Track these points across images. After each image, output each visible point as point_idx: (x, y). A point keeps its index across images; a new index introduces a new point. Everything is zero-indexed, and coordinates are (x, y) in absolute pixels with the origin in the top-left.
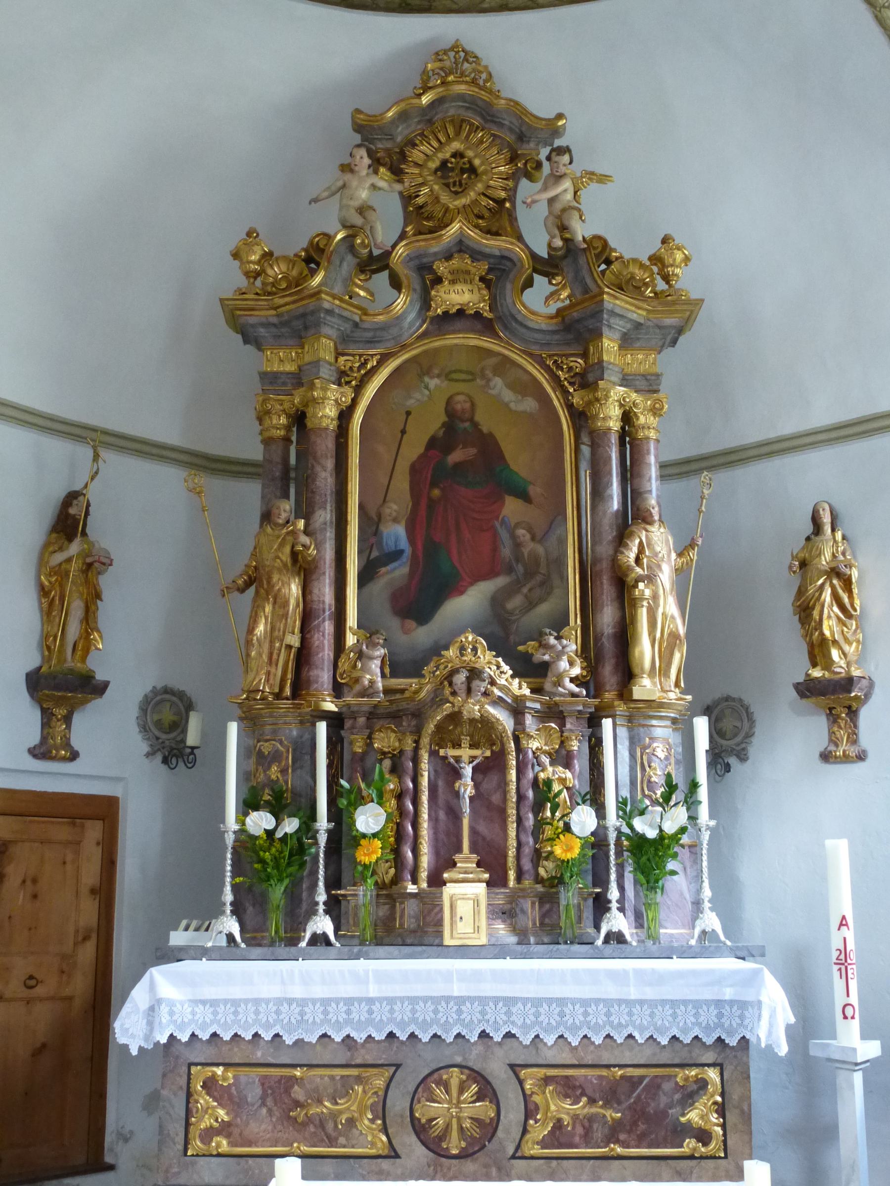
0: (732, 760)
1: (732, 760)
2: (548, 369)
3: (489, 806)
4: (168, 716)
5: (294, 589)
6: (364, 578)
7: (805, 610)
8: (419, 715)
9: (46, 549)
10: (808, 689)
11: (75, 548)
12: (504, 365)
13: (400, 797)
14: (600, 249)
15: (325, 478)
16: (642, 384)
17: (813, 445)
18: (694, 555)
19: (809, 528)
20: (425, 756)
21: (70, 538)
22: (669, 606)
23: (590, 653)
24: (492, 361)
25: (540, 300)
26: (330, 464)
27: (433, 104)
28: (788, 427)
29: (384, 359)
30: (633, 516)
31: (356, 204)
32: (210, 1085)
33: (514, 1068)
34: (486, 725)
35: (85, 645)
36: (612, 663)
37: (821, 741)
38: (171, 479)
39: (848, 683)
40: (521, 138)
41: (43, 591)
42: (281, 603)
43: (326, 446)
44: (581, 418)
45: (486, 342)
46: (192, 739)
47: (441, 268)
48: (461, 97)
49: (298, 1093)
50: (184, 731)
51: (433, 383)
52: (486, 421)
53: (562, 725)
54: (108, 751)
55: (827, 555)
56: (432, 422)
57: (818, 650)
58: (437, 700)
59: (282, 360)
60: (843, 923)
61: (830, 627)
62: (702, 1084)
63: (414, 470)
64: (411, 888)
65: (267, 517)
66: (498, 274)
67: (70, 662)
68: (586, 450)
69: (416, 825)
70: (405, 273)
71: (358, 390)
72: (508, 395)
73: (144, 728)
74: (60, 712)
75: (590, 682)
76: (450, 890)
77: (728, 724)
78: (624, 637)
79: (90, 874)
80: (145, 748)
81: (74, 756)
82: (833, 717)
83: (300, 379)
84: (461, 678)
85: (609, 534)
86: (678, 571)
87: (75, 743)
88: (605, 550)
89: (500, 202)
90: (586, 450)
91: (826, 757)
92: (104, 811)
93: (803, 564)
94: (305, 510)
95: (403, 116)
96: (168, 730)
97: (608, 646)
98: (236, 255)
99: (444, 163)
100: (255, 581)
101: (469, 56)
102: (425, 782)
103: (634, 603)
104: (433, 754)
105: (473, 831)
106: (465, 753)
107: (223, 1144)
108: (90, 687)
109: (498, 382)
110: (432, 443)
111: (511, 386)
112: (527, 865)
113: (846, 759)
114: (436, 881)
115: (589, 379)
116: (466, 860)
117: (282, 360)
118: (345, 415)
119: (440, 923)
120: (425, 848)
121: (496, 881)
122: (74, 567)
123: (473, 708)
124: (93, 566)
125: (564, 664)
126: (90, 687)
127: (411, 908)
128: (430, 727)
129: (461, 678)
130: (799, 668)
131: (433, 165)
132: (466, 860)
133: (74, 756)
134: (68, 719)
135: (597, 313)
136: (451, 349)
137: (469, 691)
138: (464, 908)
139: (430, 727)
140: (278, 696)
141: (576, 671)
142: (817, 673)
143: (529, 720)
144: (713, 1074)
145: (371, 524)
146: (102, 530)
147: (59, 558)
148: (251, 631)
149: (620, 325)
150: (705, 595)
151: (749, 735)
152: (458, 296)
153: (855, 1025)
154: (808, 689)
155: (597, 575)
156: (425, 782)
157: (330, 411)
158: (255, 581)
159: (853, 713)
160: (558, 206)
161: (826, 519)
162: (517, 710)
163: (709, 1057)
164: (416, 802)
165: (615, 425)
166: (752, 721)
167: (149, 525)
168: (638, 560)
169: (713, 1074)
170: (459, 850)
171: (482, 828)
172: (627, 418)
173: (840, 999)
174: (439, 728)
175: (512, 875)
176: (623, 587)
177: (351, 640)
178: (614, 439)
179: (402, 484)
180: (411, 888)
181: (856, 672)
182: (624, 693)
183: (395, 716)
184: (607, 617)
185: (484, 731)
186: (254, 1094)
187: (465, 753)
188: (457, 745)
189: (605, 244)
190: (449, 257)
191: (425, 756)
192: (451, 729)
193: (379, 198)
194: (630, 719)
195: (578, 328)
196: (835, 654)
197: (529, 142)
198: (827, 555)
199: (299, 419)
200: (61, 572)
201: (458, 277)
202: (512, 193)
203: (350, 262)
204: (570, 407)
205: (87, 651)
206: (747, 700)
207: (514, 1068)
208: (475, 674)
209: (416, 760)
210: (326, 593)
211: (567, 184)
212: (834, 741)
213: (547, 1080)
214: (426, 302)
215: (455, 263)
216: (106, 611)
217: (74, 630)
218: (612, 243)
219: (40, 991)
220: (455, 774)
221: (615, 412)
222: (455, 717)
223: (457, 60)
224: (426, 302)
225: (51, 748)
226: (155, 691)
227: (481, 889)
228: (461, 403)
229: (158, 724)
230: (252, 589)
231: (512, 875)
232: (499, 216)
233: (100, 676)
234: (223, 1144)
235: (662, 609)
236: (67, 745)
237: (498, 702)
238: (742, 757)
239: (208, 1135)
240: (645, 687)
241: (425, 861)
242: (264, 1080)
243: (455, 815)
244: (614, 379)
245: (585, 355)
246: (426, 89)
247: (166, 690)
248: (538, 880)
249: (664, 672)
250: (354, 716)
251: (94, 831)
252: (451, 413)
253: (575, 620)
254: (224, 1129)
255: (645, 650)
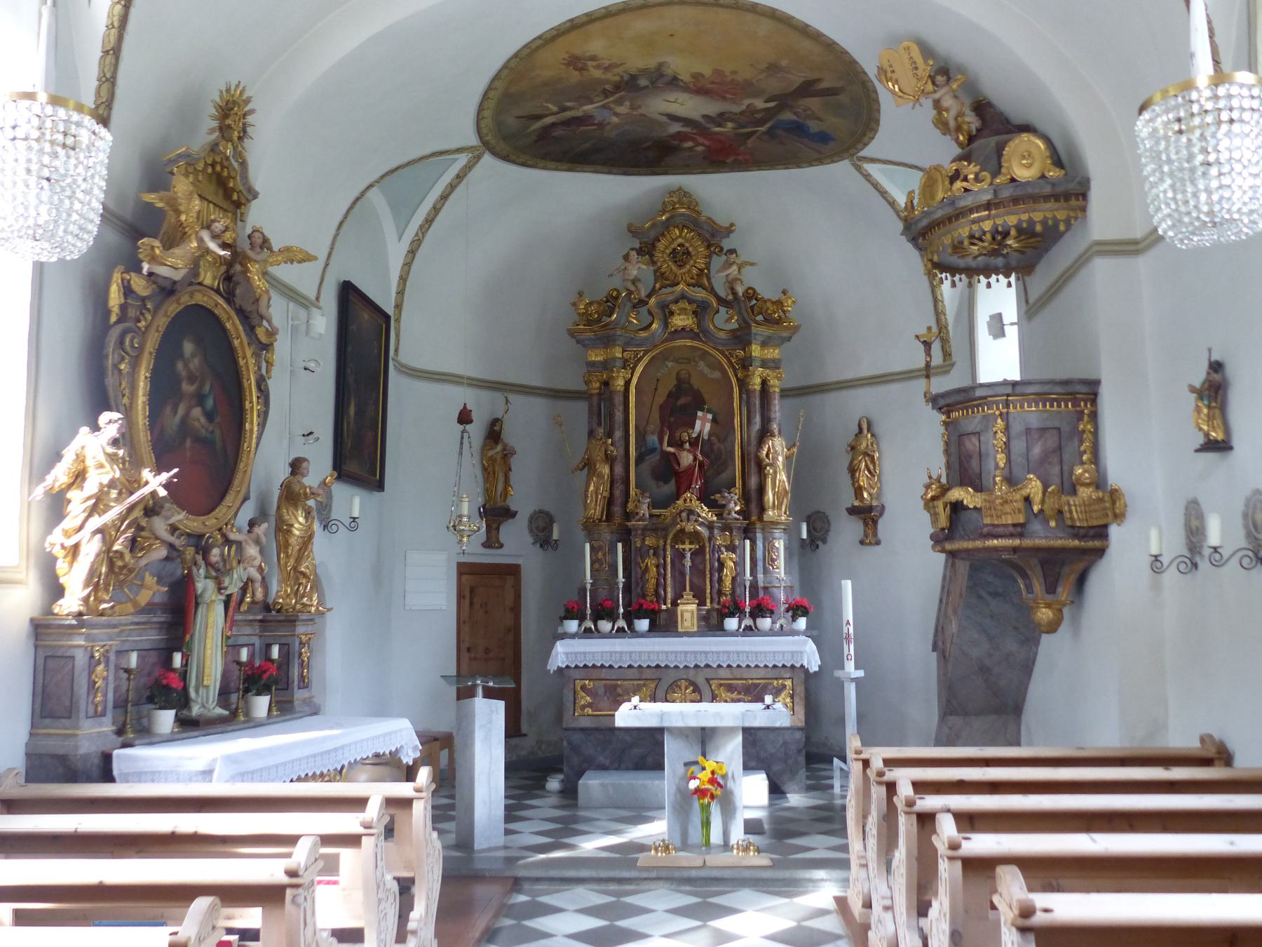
0: (820, 543)
1: (820, 543)
2: (725, 356)
3: (698, 571)
4: (541, 524)
5: (606, 470)
6: (639, 461)
7: (853, 471)
8: (666, 530)
9: (484, 448)
10: (853, 511)
11: (499, 448)
12: (705, 354)
13: (657, 567)
14: (751, 294)
15: (619, 415)
16: (772, 365)
17: (862, 385)
18: (795, 450)
19: (857, 430)
20: (668, 547)
21: (497, 443)
22: (782, 476)
23: (745, 497)
24: (699, 353)
25: (724, 322)
26: (621, 408)
27: (667, 219)
28: (850, 375)
29: (646, 353)
30: (765, 433)
31: (632, 277)
32: (583, 688)
33: (708, 680)
34: (697, 533)
35: (505, 494)
36: (754, 501)
37: (861, 535)
38: (538, 405)
39: (871, 508)
40: (713, 235)
41: (484, 469)
42: (600, 476)
43: (618, 399)
44: (743, 384)
45: (696, 344)
46: (555, 536)
47: (674, 307)
48: (682, 215)
49: (619, 691)
50: (551, 531)
51: (670, 364)
52: (696, 383)
53: (731, 533)
54: (516, 543)
55: (864, 445)
56: (669, 385)
57: (858, 491)
58: (674, 523)
59: (596, 356)
60: (848, 623)
61: (863, 482)
62: (784, 687)
63: (661, 408)
64: (664, 607)
65: (591, 434)
66: (701, 311)
67: (500, 503)
68: (744, 396)
69: (665, 579)
70: (655, 311)
71: (633, 370)
72: (706, 370)
73: (531, 531)
74: (495, 526)
75: (744, 513)
76: (680, 608)
77: (818, 525)
78: (761, 490)
79: (509, 602)
80: (531, 540)
81: (501, 546)
82: (866, 524)
83: (606, 365)
84: (684, 515)
85: (754, 442)
86: (788, 458)
87: (502, 539)
88: (753, 449)
89: (701, 270)
90: (744, 396)
91: (862, 543)
92: (513, 571)
93: (853, 448)
94: (610, 434)
95: (653, 226)
96: (541, 529)
97: (754, 495)
98: (574, 304)
99: (674, 249)
100: (588, 465)
101: (686, 194)
102: (669, 560)
103: (765, 476)
104: (673, 547)
105: (691, 582)
106: (687, 546)
107: (590, 711)
108: (509, 514)
109: (701, 363)
110: (670, 395)
111: (708, 366)
112: (715, 596)
113: (870, 544)
114: (675, 604)
115: (746, 363)
116: (688, 595)
117: (596, 356)
118: (628, 383)
119: (676, 622)
120: (669, 589)
121: (702, 603)
122: (499, 457)
123: (689, 527)
124: (507, 454)
125: (732, 505)
126: (509, 514)
127: (663, 616)
128: (671, 536)
129: (684, 515)
130: (850, 500)
131: (668, 251)
132: (688, 595)
133: (501, 546)
134: (498, 529)
135: (749, 334)
136: (679, 347)
137: (688, 520)
138: (687, 616)
139: (671, 536)
140: (600, 520)
141: (738, 508)
142: (857, 503)
143: (716, 531)
144: (788, 683)
145: (641, 435)
146: (511, 435)
147: (491, 453)
148: (587, 490)
149: (760, 339)
150: (801, 470)
151: (828, 531)
152: (679, 321)
153: (852, 663)
154: (853, 511)
155: (749, 461)
156: (669, 560)
157: (621, 382)
158: (588, 465)
159: (875, 522)
160: (731, 277)
161: (865, 427)
162: (710, 526)
163: (787, 675)
164: (665, 569)
165: (758, 388)
166: (828, 522)
167: (528, 425)
168: (767, 455)
169: (788, 683)
170: (685, 590)
171: (695, 580)
172: (764, 383)
173: (846, 652)
174: (676, 535)
175: (708, 601)
176: (761, 467)
177: (632, 493)
178: (757, 394)
179: (656, 415)
180: (664, 607)
181: (875, 503)
182: (760, 519)
183: (655, 530)
184: (753, 481)
185: (695, 536)
186: (601, 691)
187: (687, 546)
188: (683, 543)
189: (755, 291)
190: (676, 302)
191: (668, 547)
192: (681, 536)
193: (639, 269)
194: (763, 529)
195: (741, 338)
196: (865, 495)
197: (714, 236)
198: (864, 445)
199: (606, 384)
200: (492, 460)
201: (683, 311)
202: (708, 266)
203: (629, 305)
204: (738, 379)
205: (506, 497)
206: (828, 513)
207: (708, 680)
208: (691, 512)
209: (665, 550)
210: (619, 469)
211: (735, 267)
212: (866, 535)
213: (721, 685)
214: (666, 324)
215: (681, 305)
216: (513, 477)
217: (500, 487)
218: (758, 290)
219: (491, 655)
220: (683, 556)
221: (758, 381)
222: (682, 531)
223: (682, 195)
224: (666, 324)
225: (492, 542)
226: (535, 512)
227: (694, 607)
228: (684, 375)
229: (537, 528)
230: (586, 470)
231: (708, 601)
232: (701, 278)
233: (513, 508)
234: (590, 711)
235: (779, 478)
236: (498, 541)
237: (701, 524)
238: (824, 541)
239: (583, 707)
240: (770, 514)
241: (669, 595)
242: (605, 686)
243: (683, 574)
244: (758, 364)
245: (744, 350)
246: (664, 212)
247: (541, 512)
248: (719, 603)
249: (779, 508)
250: (636, 530)
251: (510, 580)
252: (678, 378)
253: (738, 482)
254: (590, 705)
255: (770, 496)
